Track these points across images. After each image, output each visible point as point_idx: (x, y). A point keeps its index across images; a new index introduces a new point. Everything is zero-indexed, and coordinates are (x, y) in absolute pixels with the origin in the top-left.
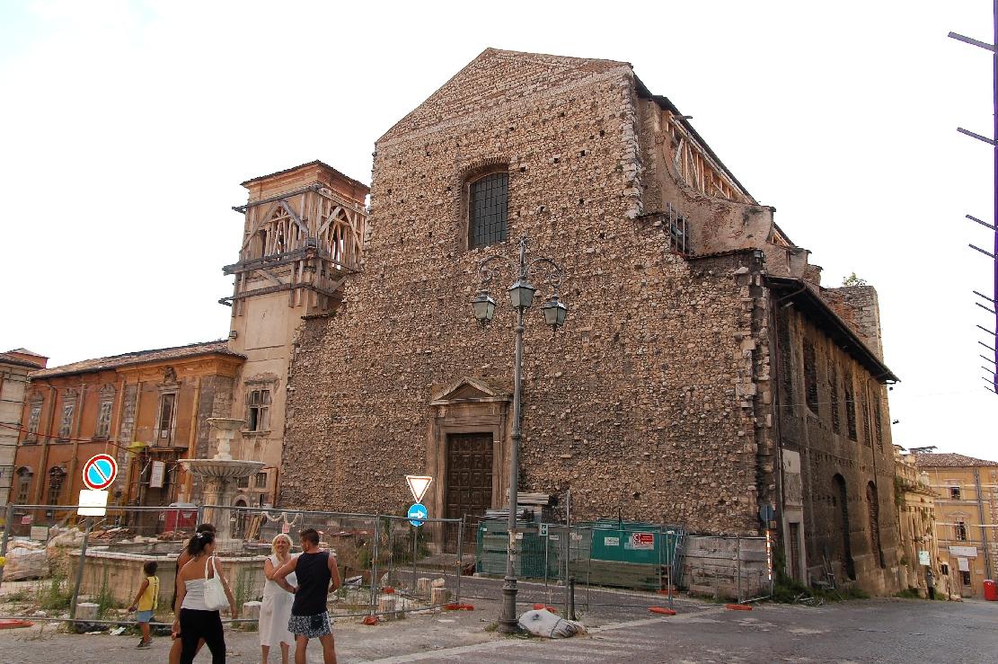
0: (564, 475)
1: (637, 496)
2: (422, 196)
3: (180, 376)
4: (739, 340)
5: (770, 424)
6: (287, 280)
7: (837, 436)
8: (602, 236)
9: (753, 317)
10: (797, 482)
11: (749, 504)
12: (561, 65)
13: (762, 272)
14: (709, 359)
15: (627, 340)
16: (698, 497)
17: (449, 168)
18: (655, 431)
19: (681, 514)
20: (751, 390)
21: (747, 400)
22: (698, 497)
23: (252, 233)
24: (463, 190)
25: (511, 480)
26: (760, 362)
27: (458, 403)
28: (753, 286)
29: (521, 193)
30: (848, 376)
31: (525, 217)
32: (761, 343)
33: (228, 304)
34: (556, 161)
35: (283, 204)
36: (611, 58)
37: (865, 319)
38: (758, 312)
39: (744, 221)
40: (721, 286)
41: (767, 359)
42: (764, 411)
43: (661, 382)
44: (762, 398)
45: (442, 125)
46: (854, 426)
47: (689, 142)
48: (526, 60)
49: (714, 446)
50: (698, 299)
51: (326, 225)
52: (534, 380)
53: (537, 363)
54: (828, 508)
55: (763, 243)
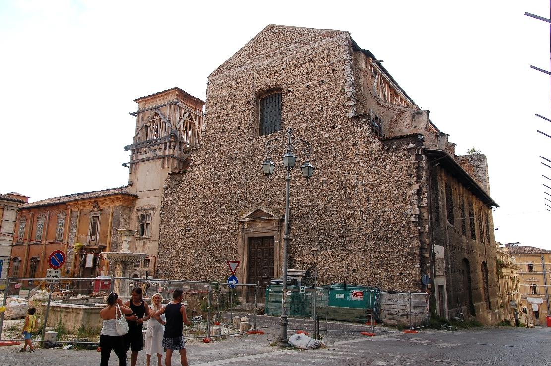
1: (354, 271)
4: (410, 185)
5: (427, 230)
6: (160, 153)
7: (465, 237)
8: (334, 127)
9: (417, 172)
11: (416, 275)
15: (348, 185)
16: (387, 271)
17: (249, 91)
19: (378, 281)
20: (417, 212)
21: (414, 218)
22: (387, 271)
26: (421, 197)
28: (417, 155)
30: (470, 204)
33: (128, 167)
47: (381, 75)
49: (397, 243)
55: (423, 130)
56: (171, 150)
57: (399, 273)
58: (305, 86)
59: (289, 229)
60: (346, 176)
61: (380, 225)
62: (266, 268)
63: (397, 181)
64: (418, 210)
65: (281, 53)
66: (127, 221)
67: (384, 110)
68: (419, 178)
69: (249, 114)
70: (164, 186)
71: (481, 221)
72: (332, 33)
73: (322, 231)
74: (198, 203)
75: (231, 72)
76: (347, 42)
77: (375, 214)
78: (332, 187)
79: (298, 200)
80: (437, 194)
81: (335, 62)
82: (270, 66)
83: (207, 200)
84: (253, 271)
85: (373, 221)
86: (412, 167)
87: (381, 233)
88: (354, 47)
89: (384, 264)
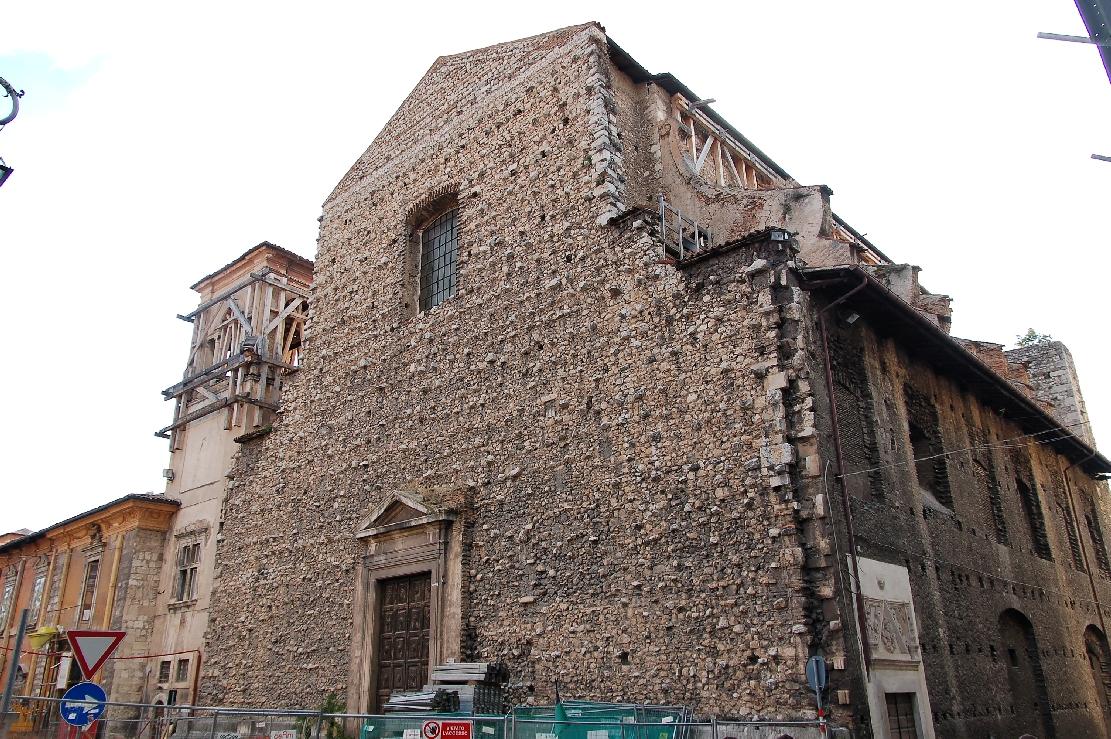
0: (523, 631)
1: (624, 657)
2: (366, 259)
3: (106, 534)
4: (760, 376)
5: (820, 510)
6: (227, 394)
7: (1003, 548)
8: (569, 259)
9: (780, 337)
10: (906, 619)
11: (796, 658)
12: (518, 51)
13: (791, 264)
14: (719, 414)
15: (604, 405)
16: (714, 653)
17: (396, 210)
18: (647, 544)
19: (690, 686)
20: (784, 454)
21: (780, 473)
22: (714, 653)
23: (198, 345)
24: (412, 238)
25: (454, 644)
26: (797, 408)
27: (387, 533)
28: (776, 289)
29: (472, 226)
30: (1019, 459)
31: (477, 255)
32: (798, 377)
33: (167, 437)
34: (513, 173)
35: (230, 303)
36: (564, 25)
37: (1055, 388)
38: (789, 328)
39: (785, 214)
40: (729, 297)
41: (809, 401)
42: (811, 490)
43: (652, 463)
44: (804, 467)
45: (390, 164)
46: (1045, 536)
47: (723, 143)
48: (479, 57)
49: (735, 559)
50: (699, 322)
51: (279, 322)
52: (485, 485)
53: (490, 458)
54: (991, 668)
55: (815, 239)
56: (248, 385)
57: (749, 658)
58: (506, 173)
59: (468, 547)
60: (597, 380)
61: (687, 508)
62: (414, 665)
63: (726, 372)
64: (786, 448)
65: (460, 113)
66: (152, 565)
67: (714, 206)
68: (785, 353)
69: (383, 264)
70: (226, 474)
71: (1069, 514)
72: (562, 36)
73: (543, 544)
74: (286, 504)
75: (365, 182)
76: (594, 46)
77: (673, 476)
78: (566, 418)
79: (490, 464)
80: (869, 407)
81: (569, 101)
82: (436, 149)
83: (305, 493)
84: (386, 676)
85: (671, 500)
86: (764, 324)
87: (697, 533)
88: (619, 61)
89: (704, 629)
